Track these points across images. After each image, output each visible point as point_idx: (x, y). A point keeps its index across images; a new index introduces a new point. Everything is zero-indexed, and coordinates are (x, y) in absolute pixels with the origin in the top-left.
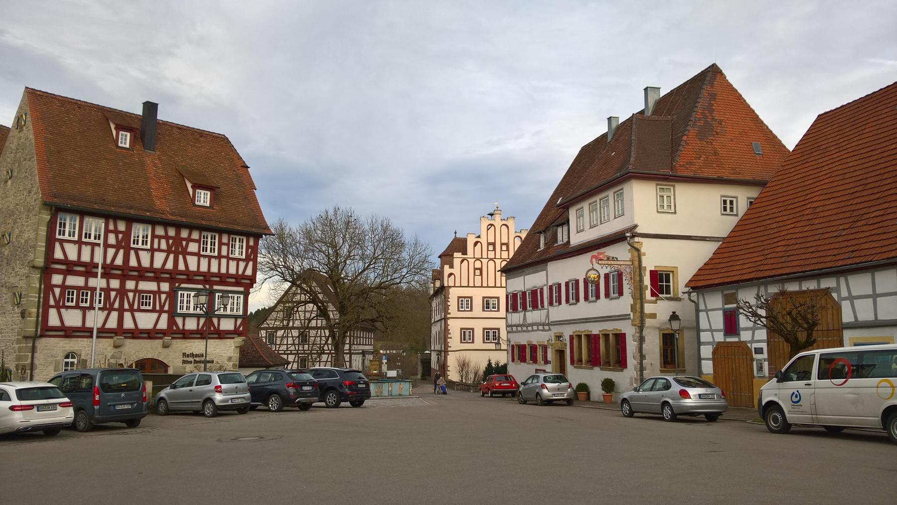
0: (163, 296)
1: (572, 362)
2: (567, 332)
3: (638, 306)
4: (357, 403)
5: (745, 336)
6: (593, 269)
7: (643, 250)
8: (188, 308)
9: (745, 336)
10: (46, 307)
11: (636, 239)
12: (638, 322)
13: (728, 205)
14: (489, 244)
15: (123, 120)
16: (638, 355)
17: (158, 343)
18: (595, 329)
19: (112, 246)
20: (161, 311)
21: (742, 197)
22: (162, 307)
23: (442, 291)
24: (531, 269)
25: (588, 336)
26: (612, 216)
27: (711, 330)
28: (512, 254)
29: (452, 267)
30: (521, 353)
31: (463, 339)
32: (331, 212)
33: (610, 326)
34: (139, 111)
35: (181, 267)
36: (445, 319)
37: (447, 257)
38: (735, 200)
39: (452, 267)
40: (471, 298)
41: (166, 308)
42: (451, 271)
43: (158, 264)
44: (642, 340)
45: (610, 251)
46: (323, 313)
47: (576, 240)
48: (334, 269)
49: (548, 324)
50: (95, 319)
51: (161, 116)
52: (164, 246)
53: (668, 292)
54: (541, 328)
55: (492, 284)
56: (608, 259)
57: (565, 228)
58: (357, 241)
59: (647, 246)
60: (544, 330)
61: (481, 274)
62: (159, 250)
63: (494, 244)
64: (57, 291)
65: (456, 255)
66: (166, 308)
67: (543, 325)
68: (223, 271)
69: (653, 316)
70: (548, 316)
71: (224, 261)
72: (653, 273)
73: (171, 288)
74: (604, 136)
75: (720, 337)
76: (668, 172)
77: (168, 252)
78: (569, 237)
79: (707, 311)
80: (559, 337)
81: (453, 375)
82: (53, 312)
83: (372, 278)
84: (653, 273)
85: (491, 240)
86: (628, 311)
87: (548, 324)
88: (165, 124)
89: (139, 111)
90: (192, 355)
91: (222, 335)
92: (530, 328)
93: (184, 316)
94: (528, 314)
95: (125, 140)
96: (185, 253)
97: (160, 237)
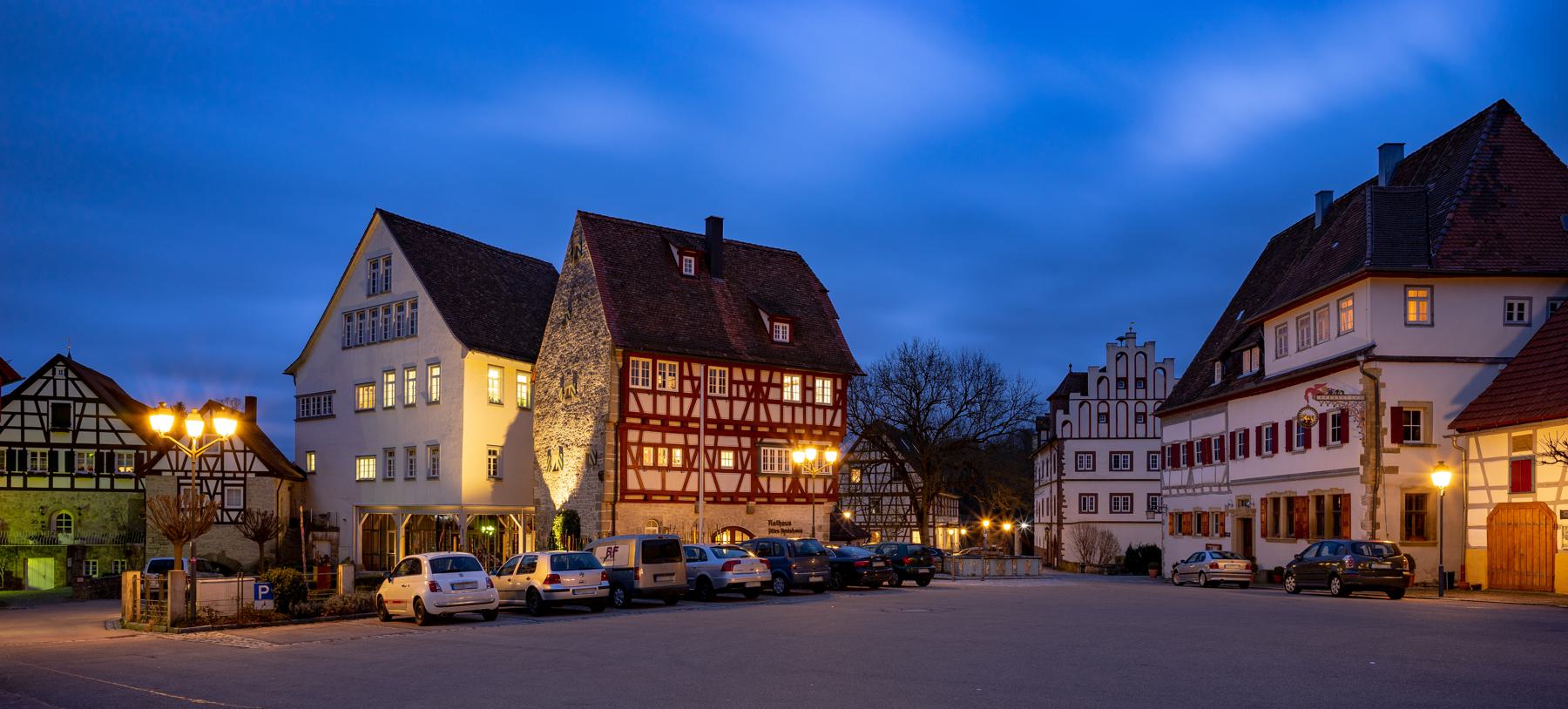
0: (745, 454)
1: (1264, 535)
2: (1257, 494)
3: (1372, 457)
4: (923, 581)
5: (1543, 495)
6: (1308, 407)
7: (1381, 380)
8: (772, 467)
9: (1543, 495)
10: (625, 467)
11: (1373, 365)
12: (1370, 476)
13: (1515, 311)
14: (1118, 380)
15: (684, 241)
16: (1369, 524)
17: (741, 509)
18: (1301, 489)
19: (688, 395)
20: (743, 472)
21: (1538, 297)
22: (744, 466)
23: (1055, 443)
24: (1201, 411)
25: (1291, 501)
26: (1334, 333)
27: (1488, 488)
28: (1169, 391)
29: (1067, 412)
30: (1183, 524)
31: (1083, 508)
32: (910, 344)
33: (1326, 486)
34: (701, 230)
35: (763, 418)
36: (1059, 482)
37: (1059, 399)
38: (1526, 304)
39: (1067, 412)
40: (1094, 453)
41: (749, 467)
42: (1067, 417)
43: (737, 416)
44: (1375, 502)
45: (1332, 381)
46: (900, 475)
47: (1273, 368)
48: (916, 421)
49: (1228, 484)
50: (675, 482)
51: (727, 235)
52: (743, 394)
53: (1417, 437)
54: (1215, 489)
55: (1122, 433)
56: (1330, 393)
57: (1256, 351)
58: (945, 379)
59: (1387, 373)
60: (1219, 493)
61: (1108, 421)
62: (738, 398)
63: (1126, 380)
64: (634, 449)
65: (1072, 396)
66: (749, 467)
67: (1210, 485)
68: (809, 422)
69: (1394, 470)
70: (1227, 473)
71: (809, 409)
72: (1397, 412)
73: (753, 443)
74: (1310, 220)
75: (1502, 497)
76: (1424, 266)
77: (748, 400)
78: (1262, 364)
79: (1481, 461)
80: (1243, 502)
81: (1070, 553)
82: (631, 473)
83: (967, 425)
84: (1397, 412)
85: (1122, 374)
86: (1356, 463)
87: (1228, 484)
88: (730, 243)
89: (701, 230)
90: (779, 523)
91: (809, 499)
92: (1198, 490)
93: (769, 476)
94: (1166, 474)
95: (689, 266)
96: (766, 401)
97: (738, 383)
